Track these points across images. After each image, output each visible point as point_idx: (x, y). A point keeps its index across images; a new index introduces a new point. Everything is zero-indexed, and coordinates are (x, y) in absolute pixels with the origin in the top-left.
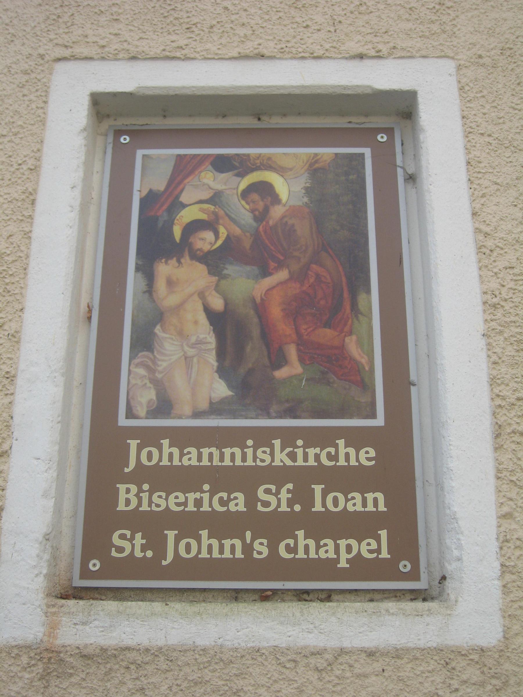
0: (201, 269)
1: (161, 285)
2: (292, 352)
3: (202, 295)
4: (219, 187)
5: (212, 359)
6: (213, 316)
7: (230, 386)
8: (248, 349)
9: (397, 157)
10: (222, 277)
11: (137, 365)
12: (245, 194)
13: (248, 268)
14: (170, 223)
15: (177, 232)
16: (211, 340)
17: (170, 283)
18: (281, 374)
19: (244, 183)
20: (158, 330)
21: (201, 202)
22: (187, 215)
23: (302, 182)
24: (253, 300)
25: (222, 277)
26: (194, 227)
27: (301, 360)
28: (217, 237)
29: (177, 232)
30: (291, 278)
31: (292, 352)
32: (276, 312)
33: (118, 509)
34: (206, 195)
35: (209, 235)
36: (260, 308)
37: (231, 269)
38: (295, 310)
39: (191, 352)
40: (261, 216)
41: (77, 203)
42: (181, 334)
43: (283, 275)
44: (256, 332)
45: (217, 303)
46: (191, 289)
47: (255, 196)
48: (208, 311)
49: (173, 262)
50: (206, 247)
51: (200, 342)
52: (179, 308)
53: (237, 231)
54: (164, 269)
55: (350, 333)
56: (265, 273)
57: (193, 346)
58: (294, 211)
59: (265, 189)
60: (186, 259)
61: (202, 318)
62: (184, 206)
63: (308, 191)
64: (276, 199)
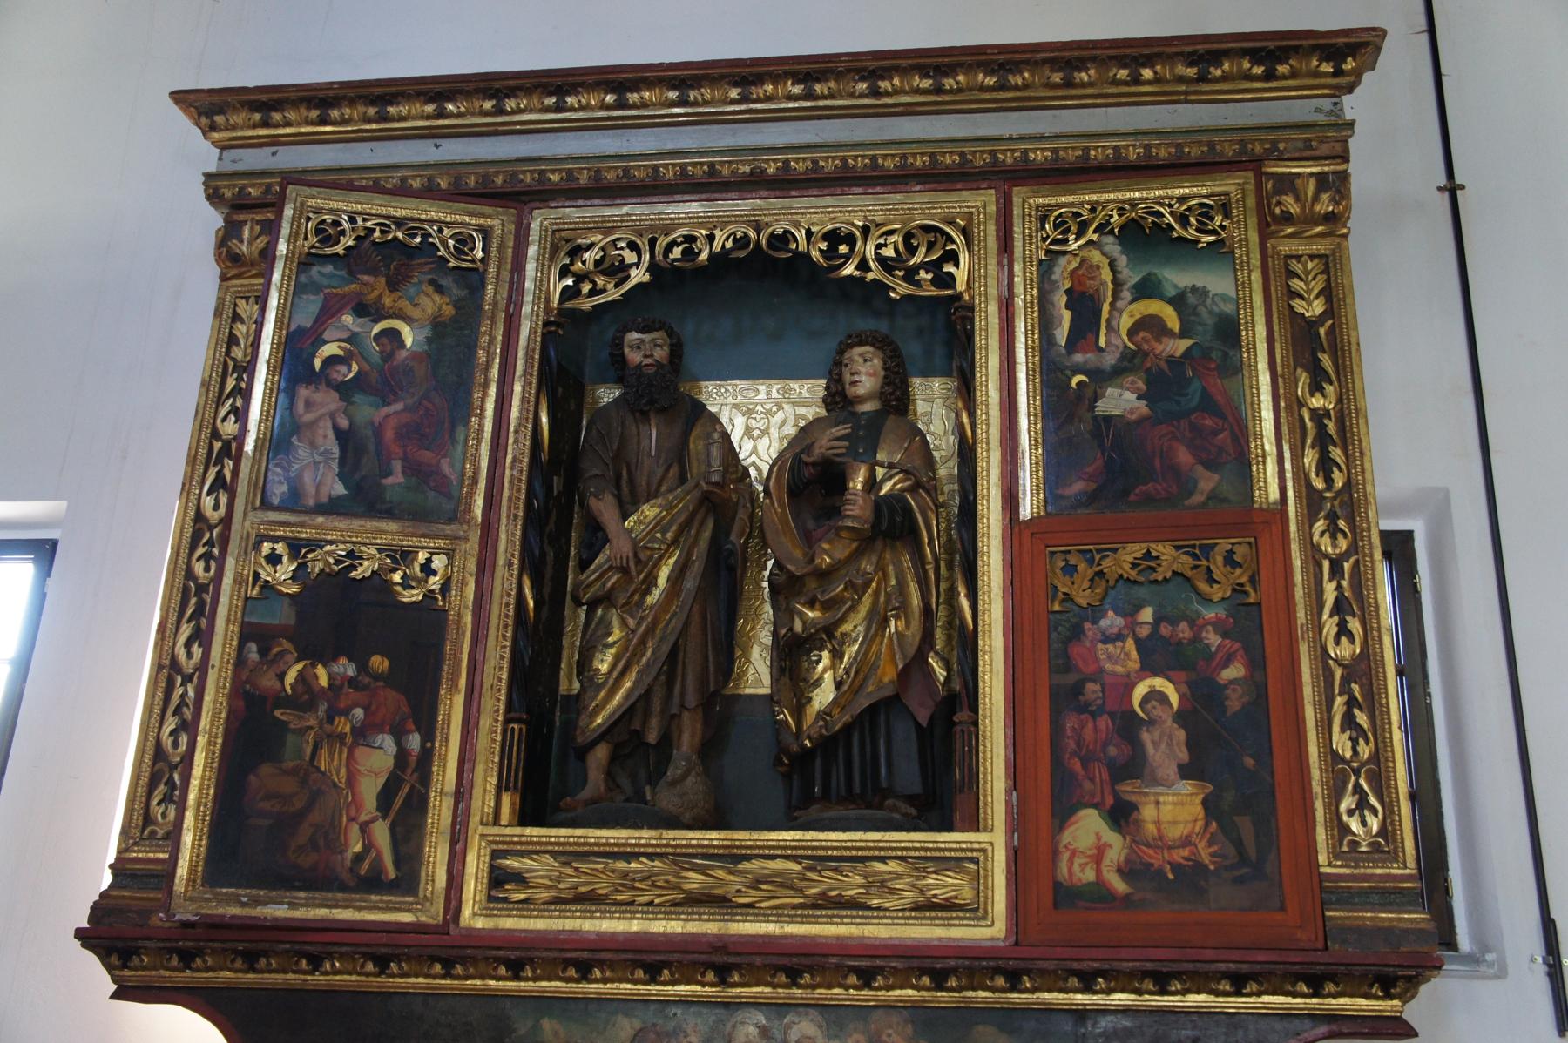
0: (336, 395)
1: (300, 406)
2: (397, 466)
3: (332, 416)
4: (357, 329)
5: (335, 466)
6: (340, 434)
7: (346, 487)
8: (364, 460)
9: (1261, 377)
10: (350, 403)
11: (277, 465)
12: (377, 338)
13: (372, 398)
14: (313, 356)
15: (318, 363)
16: (336, 450)
17: (309, 405)
18: (388, 481)
19: (377, 329)
20: (294, 439)
21: (340, 340)
22: (330, 349)
23: (426, 332)
24: (372, 423)
25: (350, 403)
26: (331, 361)
27: (404, 473)
28: (350, 371)
29: (318, 363)
30: (406, 409)
31: (397, 466)
32: (389, 434)
33: (1228, 714)
34: (345, 335)
35: (343, 369)
36: (378, 431)
37: (358, 398)
38: (404, 434)
39: (318, 459)
40: (387, 357)
41: (959, 390)
42: (313, 445)
43: (399, 406)
44: (372, 447)
45: (344, 423)
46: (323, 411)
47: (384, 340)
48: (336, 428)
49: (312, 387)
50: (340, 378)
51: (327, 452)
52: (315, 422)
53: (368, 368)
54: (303, 392)
55: (445, 456)
56: (386, 403)
57: (321, 454)
58: (414, 356)
59: (394, 335)
60: (323, 386)
61: (331, 434)
62: (326, 342)
63: (429, 340)
64: (402, 344)
